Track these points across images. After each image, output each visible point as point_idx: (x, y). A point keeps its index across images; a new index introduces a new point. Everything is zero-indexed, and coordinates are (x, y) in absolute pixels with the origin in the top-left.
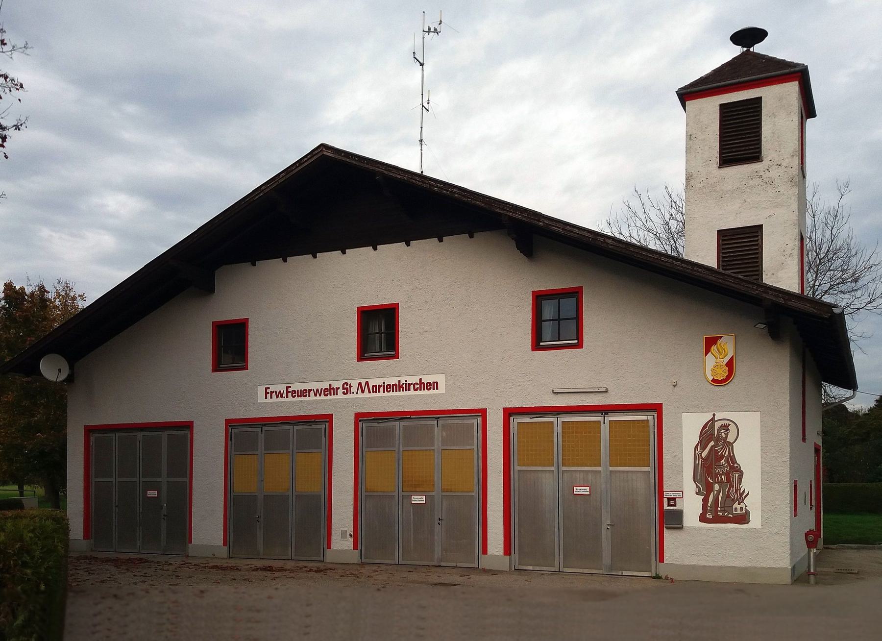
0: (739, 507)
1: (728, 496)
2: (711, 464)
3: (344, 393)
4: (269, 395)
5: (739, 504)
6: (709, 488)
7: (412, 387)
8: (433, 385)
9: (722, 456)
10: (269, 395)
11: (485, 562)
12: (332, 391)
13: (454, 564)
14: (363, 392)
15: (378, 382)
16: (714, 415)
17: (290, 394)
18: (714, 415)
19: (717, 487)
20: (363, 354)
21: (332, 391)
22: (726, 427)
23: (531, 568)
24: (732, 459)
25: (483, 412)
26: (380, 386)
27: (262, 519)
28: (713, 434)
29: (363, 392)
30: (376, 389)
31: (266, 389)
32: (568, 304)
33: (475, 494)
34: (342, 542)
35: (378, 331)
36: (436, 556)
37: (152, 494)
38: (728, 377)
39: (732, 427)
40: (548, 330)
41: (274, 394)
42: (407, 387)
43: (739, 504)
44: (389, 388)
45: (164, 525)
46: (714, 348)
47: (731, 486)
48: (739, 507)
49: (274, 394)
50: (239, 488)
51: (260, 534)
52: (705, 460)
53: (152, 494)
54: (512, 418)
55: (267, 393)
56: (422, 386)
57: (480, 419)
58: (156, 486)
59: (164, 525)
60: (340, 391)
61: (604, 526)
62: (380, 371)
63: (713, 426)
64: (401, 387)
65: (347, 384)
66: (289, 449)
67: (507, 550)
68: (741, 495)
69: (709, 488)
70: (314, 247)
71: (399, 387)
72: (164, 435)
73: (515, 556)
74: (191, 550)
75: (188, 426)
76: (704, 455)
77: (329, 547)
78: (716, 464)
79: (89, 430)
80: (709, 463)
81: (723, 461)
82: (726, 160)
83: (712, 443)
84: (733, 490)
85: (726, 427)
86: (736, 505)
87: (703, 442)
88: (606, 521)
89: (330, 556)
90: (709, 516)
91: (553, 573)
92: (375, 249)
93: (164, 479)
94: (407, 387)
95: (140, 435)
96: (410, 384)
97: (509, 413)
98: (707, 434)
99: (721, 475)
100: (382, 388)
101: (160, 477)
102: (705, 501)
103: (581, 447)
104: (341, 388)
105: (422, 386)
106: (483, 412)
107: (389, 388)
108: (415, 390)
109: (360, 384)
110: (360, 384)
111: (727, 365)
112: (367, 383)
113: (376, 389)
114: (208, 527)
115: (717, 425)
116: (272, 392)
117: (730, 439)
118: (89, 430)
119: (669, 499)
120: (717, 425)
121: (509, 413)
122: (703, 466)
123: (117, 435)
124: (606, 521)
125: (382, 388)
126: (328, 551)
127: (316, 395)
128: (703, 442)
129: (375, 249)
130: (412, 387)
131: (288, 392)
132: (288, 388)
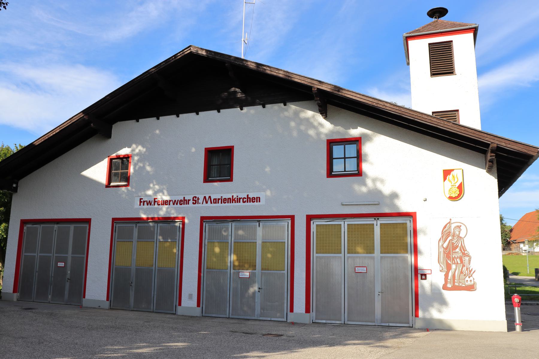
0: (469, 280)
1: (462, 272)
2: (450, 251)
3: (193, 203)
4: (142, 204)
5: (469, 277)
6: (449, 267)
7: (241, 200)
8: (258, 199)
9: (457, 247)
10: (142, 204)
11: (291, 318)
12: (185, 201)
13: (269, 319)
14: (207, 203)
15: (218, 196)
16: (451, 219)
17: (156, 203)
18: (451, 219)
19: (454, 267)
20: (207, 179)
21: (185, 201)
22: (459, 227)
23: (324, 321)
24: (463, 249)
25: (292, 218)
26: (219, 199)
27: (133, 284)
28: (450, 232)
29: (207, 203)
30: (216, 201)
31: (141, 199)
32: (351, 150)
33: (285, 272)
34: (189, 301)
35: (219, 163)
36: (256, 313)
37: (61, 264)
38: (459, 195)
39: (463, 228)
40: (214, 171)
41: (145, 203)
42: (238, 200)
43: (469, 277)
44: (225, 201)
45: (67, 285)
46: (450, 177)
47: (464, 266)
48: (469, 280)
49: (145, 203)
50: (118, 262)
51: (132, 294)
52: (446, 249)
53: (61, 264)
54: (312, 222)
55: (141, 202)
56: (249, 199)
57: (290, 222)
58: (64, 260)
59: (67, 285)
60: (191, 202)
61: (377, 293)
62: (218, 189)
63: (450, 227)
64: (234, 200)
65: (196, 197)
66: (154, 239)
67: (308, 310)
68: (470, 271)
69: (449, 267)
70: (177, 110)
71: (231, 200)
72: (72, 227)
73: (313, 314)
74: (85, 303)
75: (88, 221)
76: (445, 245)
77: (180, 304)
78: (453, 250)
79: (24, 223)
80: (448, 250)
81: (458, 250)
82: (306, 312)
83: (450, 238)
84: (464, 269)
85: (459, 227)
86: (467, 278)
87: (444, 237)
88: (378, 288)
89: (180, 310)
90: (449, 286)
91: (340, 325)
92: (219, 112)
93: (70, 255)
94: (238, 200)
95: (56, 226)
96: (240, 199)
97: (310, 218)
98: (446, 233)
99: (457, 259)
100: (220, 201)
101: (67, 253)
102: (446, 276)
103: (361, 238)
104: (192, 200)
105: (249, 199)
106: (292, 218)
107: (225, 201)
108: (244, 202)
109: (205, 197)
110: (205, 197)
111: (459, 187)
112: (210, 197)
113: (216, 201)
114: (97, 287)
115: (453, 226)
116: (144, 202)
117: (462, 235)
118: (24, 223)
119: (422, 275)
120: (453, 226)
121: (310, 218)
122: (444, 253)
123: (42, 226)
124: (378, 288)
125: (220, 201)
126: (179, 308)
127: (174, 204)
128: (444, 237)
129: (219, 112)
130: (241, 200)
131: (155, 202)
132: (155, 199)
